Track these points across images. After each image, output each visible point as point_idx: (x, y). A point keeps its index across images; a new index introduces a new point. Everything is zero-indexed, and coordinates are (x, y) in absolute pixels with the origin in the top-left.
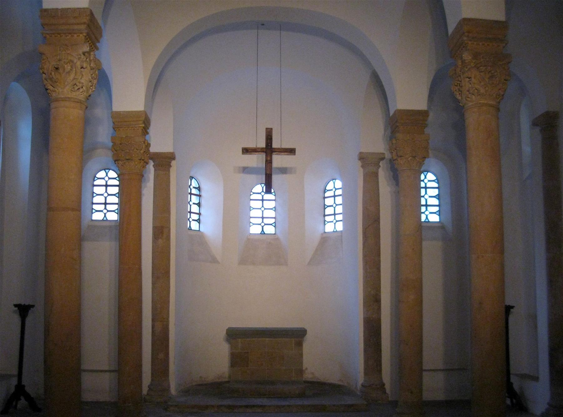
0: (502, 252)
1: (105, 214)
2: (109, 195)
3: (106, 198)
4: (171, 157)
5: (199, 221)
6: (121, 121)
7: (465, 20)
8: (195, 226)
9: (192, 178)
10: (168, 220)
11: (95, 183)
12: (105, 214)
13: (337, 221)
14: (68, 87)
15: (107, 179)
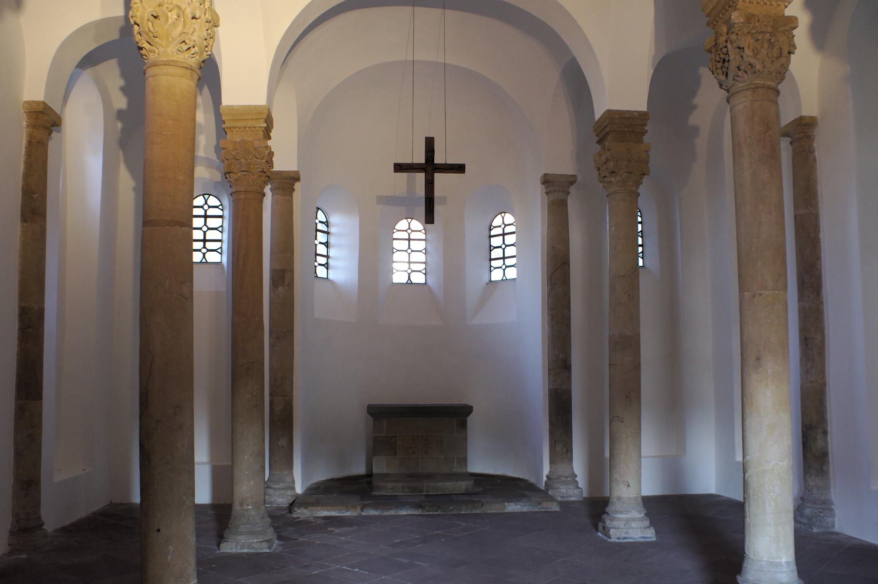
1: (204, 254)
2: (209, 229)
3: (205, 233)
5: (327, 266)
12: (204, 254)
13: (507, 267)
15: (206, 207)
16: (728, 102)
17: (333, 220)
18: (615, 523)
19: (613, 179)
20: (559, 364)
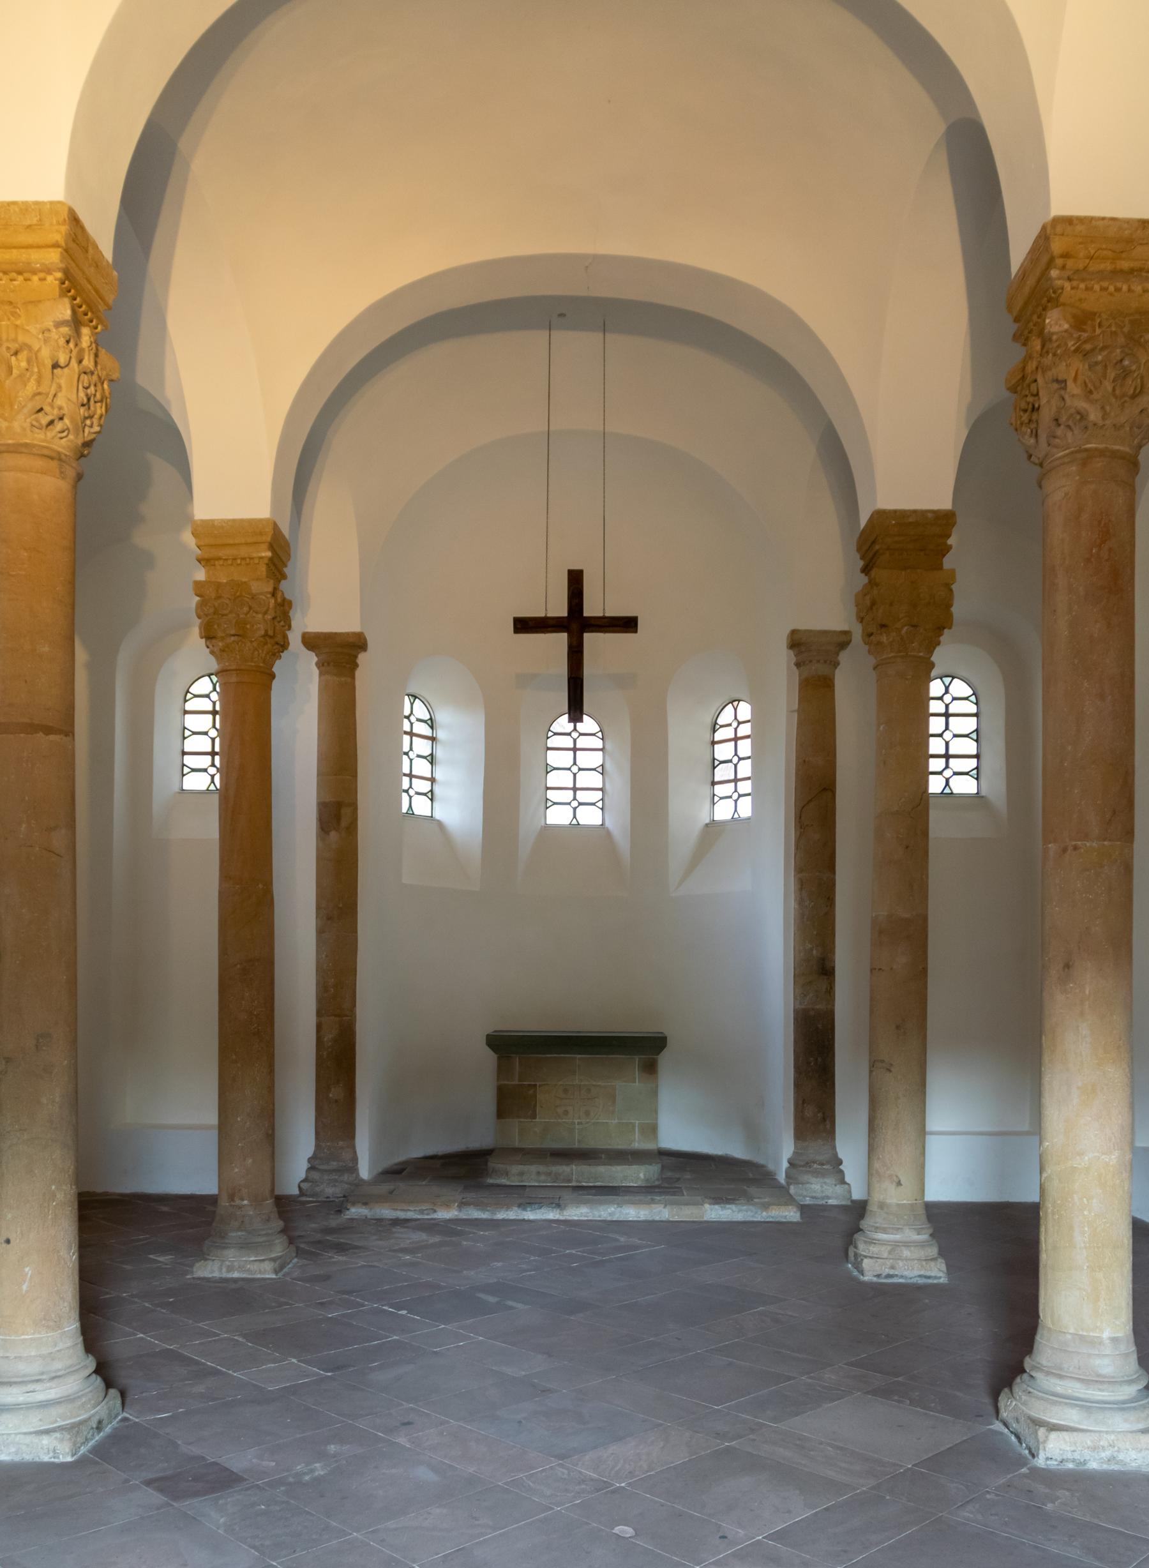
5: (431, 796)
6: (218, 542)
7: (1058, 220)
8: (422, 807)
11: (189, 706)
14: (21, 417)
16: (1040, 487)
17: (441, 717)
18: (874, 1249)
19: (884, 639)
20: (816, 968)
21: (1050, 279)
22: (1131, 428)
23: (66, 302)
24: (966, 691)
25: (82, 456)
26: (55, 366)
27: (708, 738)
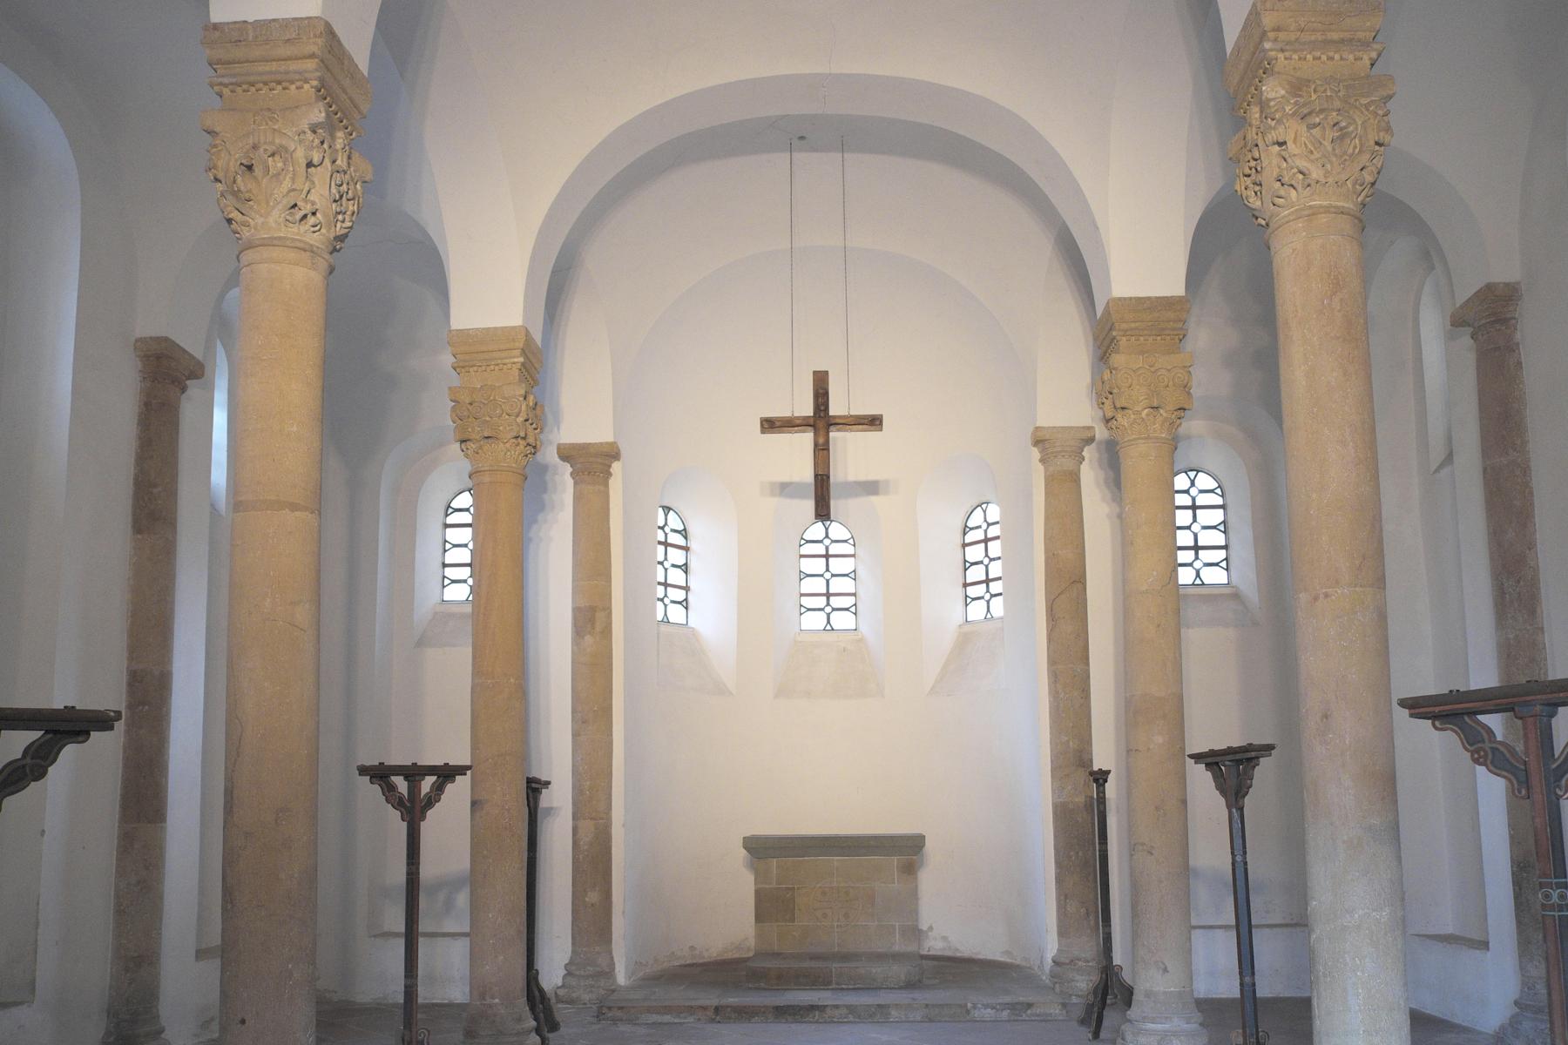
0: (1380, 582)
4: (610, 454)
5: (685, 604)
6: (475, 350)
8: (676, 614)
9: (667, 509)
10: (606, 595)
14: (275, 213)
21: (1265, 51)
22: (1354, 185)
23: (321, 105)
24: (1212, 484)
25: (335, 250)
26: (310, 165)
27: (960, 542)
